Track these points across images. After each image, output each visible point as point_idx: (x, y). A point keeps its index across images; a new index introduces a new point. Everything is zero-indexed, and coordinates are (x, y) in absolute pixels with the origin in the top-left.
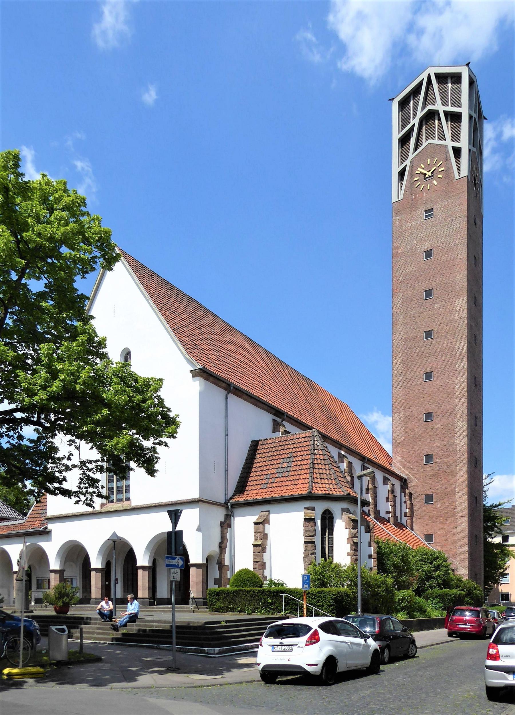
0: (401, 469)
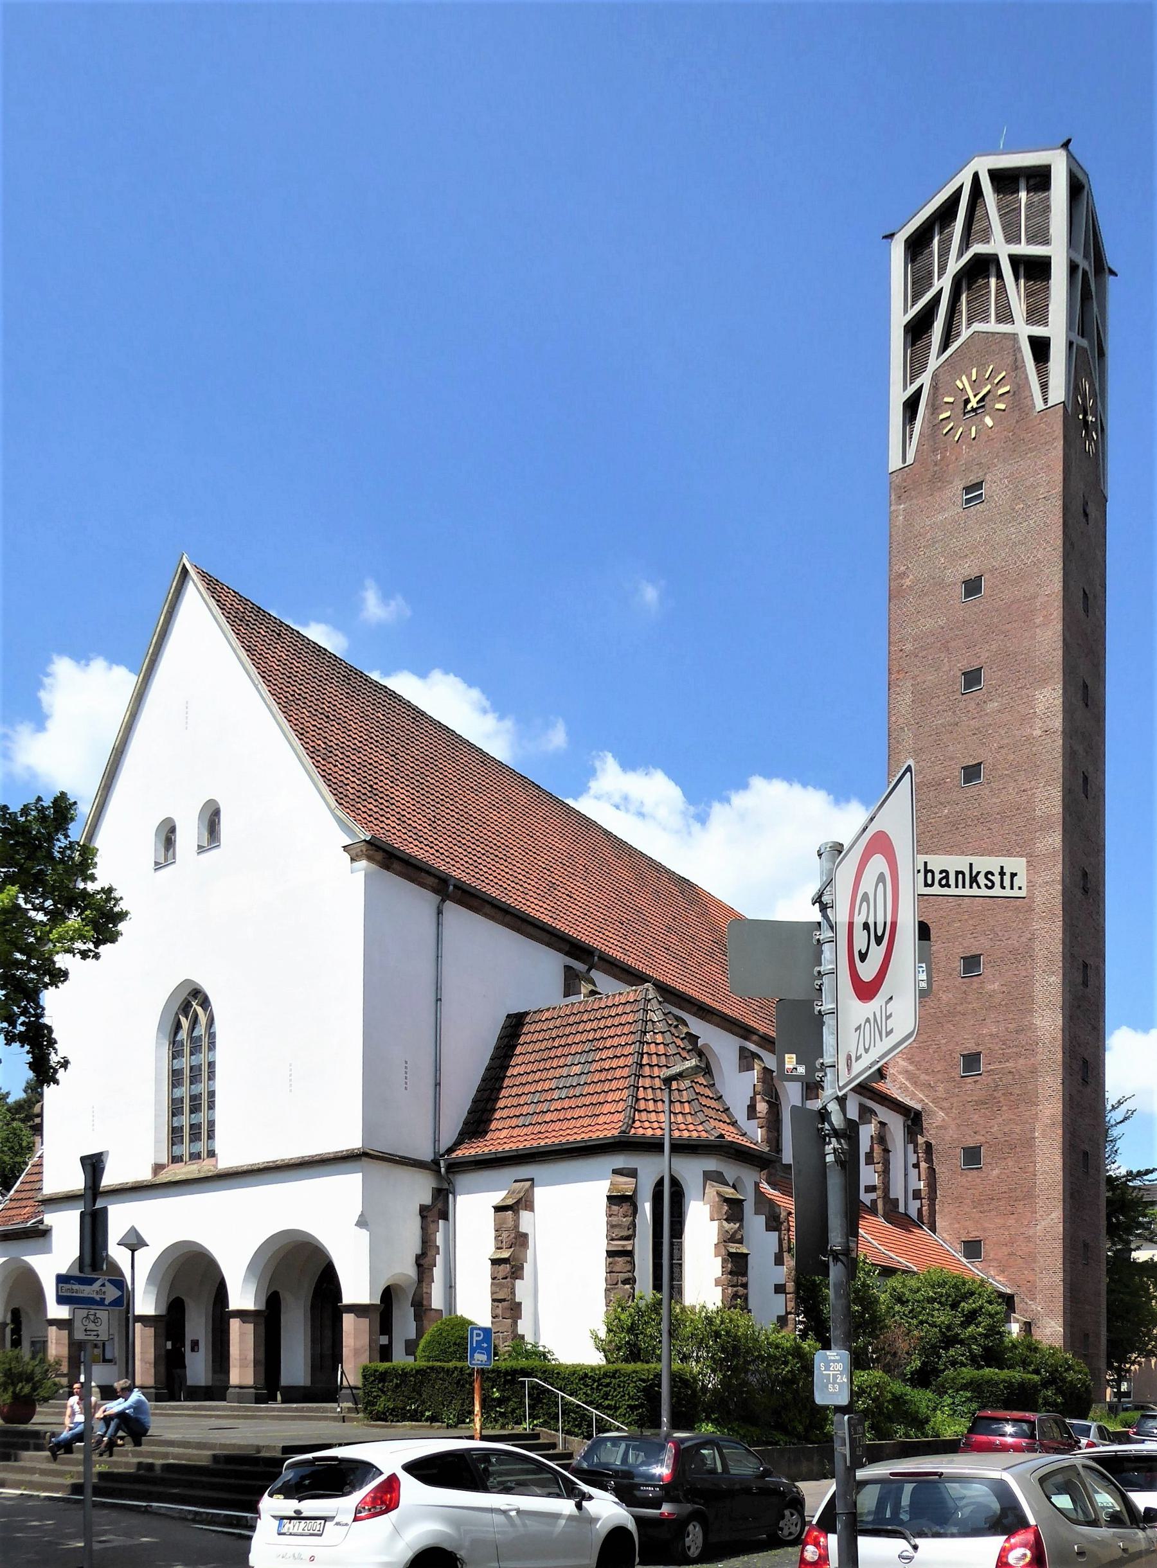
0: (906, 1089)
